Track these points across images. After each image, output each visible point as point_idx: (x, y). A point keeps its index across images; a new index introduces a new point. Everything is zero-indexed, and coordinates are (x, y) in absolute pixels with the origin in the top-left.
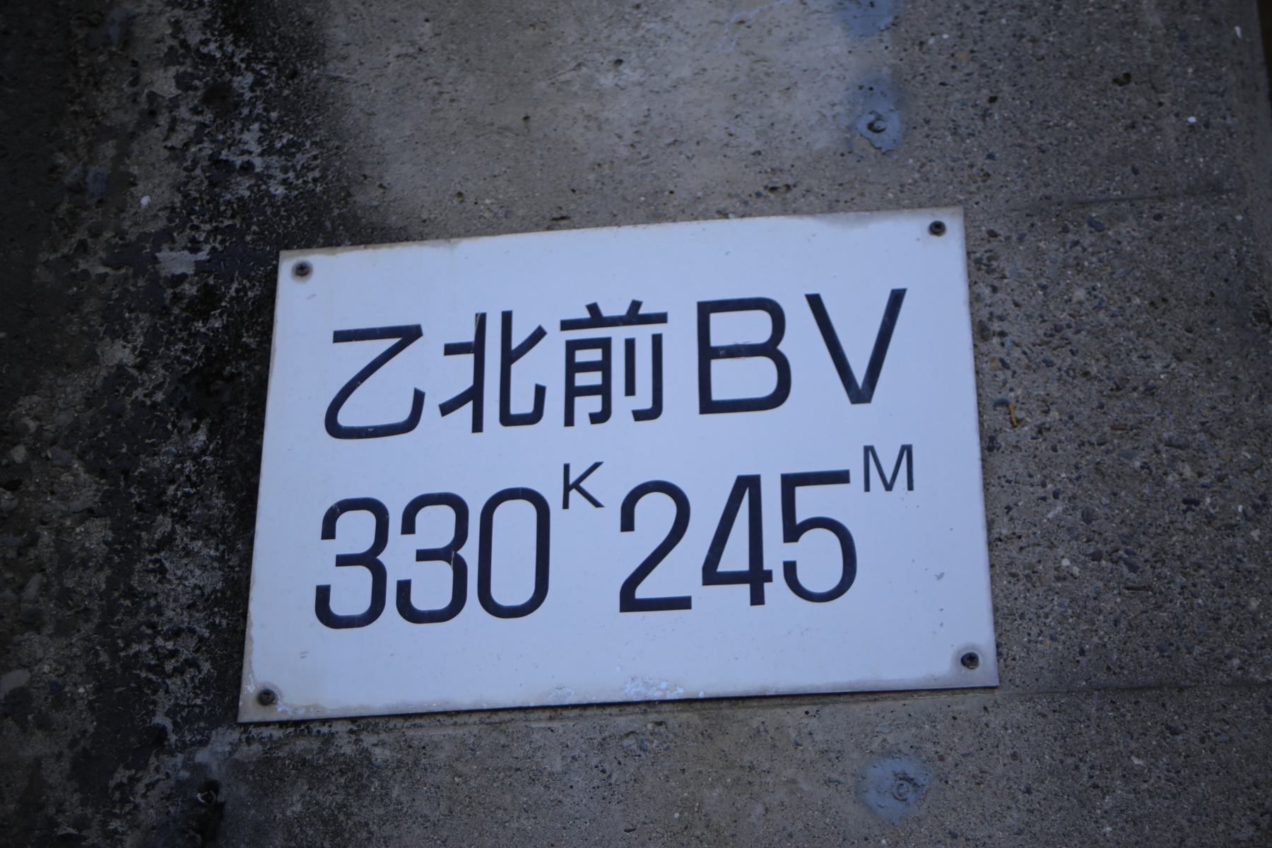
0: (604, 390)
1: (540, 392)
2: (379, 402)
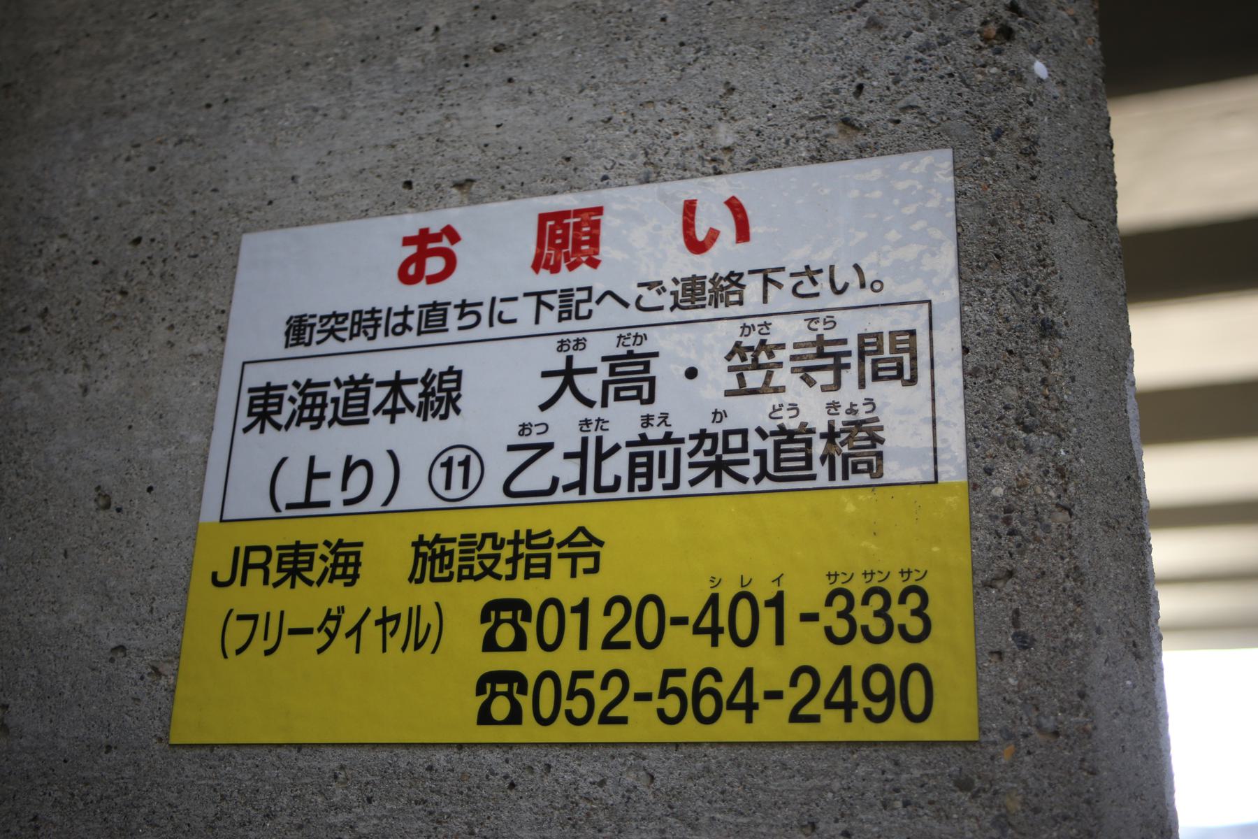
0: (649, 476)
1: (429, 626)
2: (536, 478)
